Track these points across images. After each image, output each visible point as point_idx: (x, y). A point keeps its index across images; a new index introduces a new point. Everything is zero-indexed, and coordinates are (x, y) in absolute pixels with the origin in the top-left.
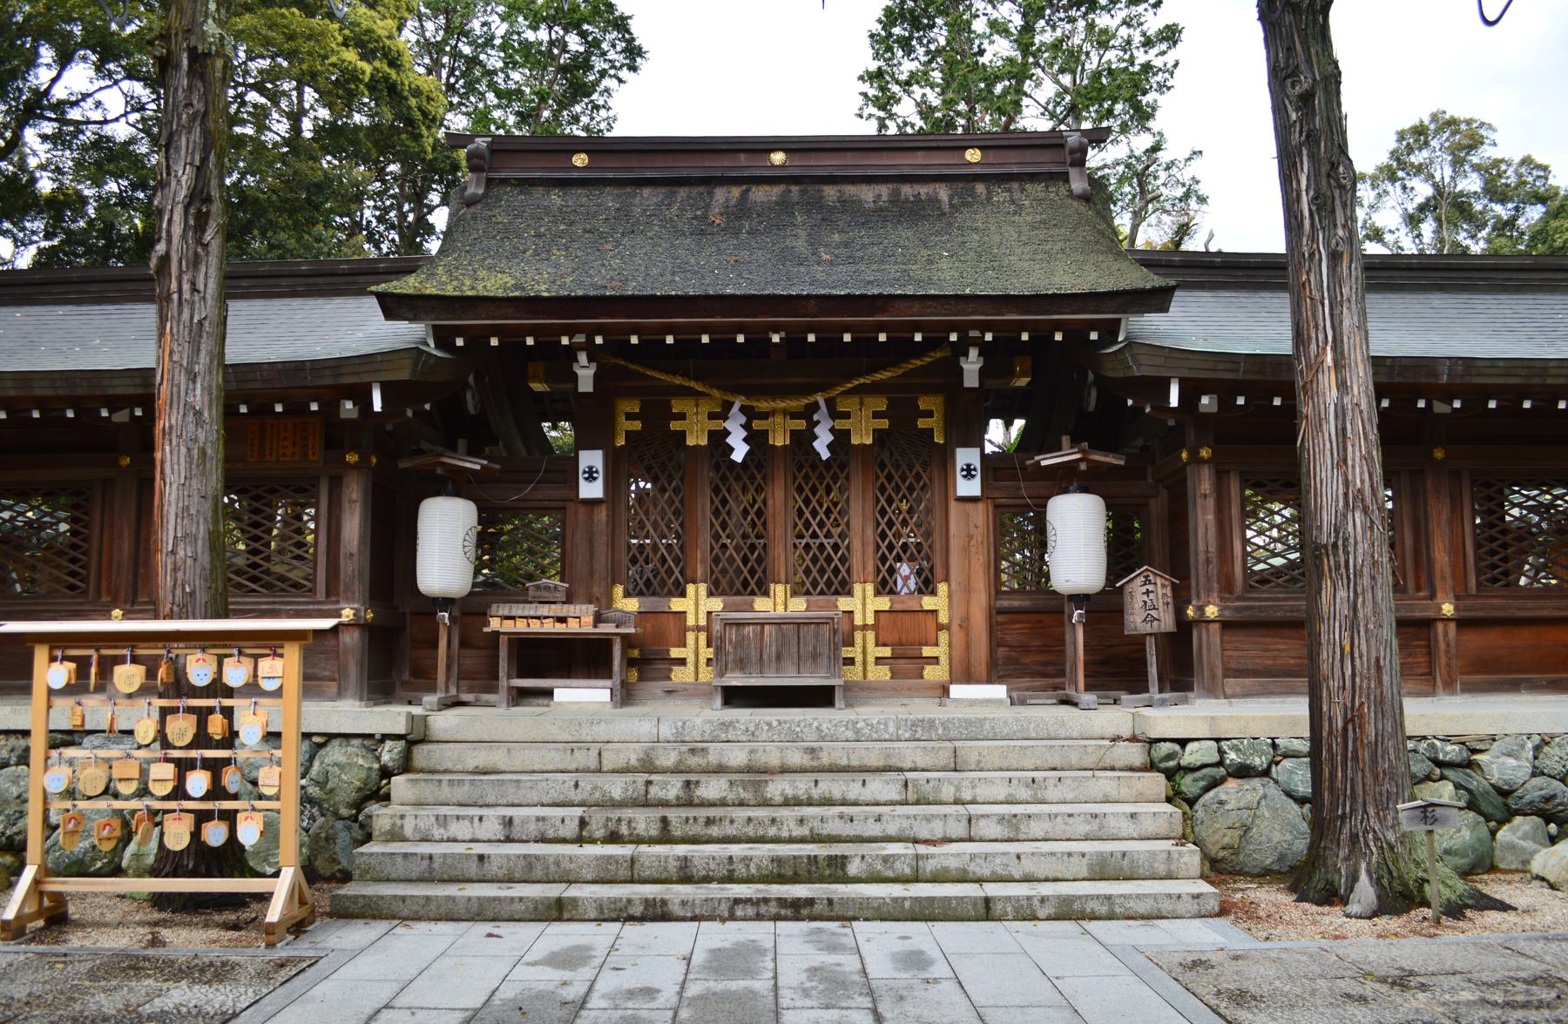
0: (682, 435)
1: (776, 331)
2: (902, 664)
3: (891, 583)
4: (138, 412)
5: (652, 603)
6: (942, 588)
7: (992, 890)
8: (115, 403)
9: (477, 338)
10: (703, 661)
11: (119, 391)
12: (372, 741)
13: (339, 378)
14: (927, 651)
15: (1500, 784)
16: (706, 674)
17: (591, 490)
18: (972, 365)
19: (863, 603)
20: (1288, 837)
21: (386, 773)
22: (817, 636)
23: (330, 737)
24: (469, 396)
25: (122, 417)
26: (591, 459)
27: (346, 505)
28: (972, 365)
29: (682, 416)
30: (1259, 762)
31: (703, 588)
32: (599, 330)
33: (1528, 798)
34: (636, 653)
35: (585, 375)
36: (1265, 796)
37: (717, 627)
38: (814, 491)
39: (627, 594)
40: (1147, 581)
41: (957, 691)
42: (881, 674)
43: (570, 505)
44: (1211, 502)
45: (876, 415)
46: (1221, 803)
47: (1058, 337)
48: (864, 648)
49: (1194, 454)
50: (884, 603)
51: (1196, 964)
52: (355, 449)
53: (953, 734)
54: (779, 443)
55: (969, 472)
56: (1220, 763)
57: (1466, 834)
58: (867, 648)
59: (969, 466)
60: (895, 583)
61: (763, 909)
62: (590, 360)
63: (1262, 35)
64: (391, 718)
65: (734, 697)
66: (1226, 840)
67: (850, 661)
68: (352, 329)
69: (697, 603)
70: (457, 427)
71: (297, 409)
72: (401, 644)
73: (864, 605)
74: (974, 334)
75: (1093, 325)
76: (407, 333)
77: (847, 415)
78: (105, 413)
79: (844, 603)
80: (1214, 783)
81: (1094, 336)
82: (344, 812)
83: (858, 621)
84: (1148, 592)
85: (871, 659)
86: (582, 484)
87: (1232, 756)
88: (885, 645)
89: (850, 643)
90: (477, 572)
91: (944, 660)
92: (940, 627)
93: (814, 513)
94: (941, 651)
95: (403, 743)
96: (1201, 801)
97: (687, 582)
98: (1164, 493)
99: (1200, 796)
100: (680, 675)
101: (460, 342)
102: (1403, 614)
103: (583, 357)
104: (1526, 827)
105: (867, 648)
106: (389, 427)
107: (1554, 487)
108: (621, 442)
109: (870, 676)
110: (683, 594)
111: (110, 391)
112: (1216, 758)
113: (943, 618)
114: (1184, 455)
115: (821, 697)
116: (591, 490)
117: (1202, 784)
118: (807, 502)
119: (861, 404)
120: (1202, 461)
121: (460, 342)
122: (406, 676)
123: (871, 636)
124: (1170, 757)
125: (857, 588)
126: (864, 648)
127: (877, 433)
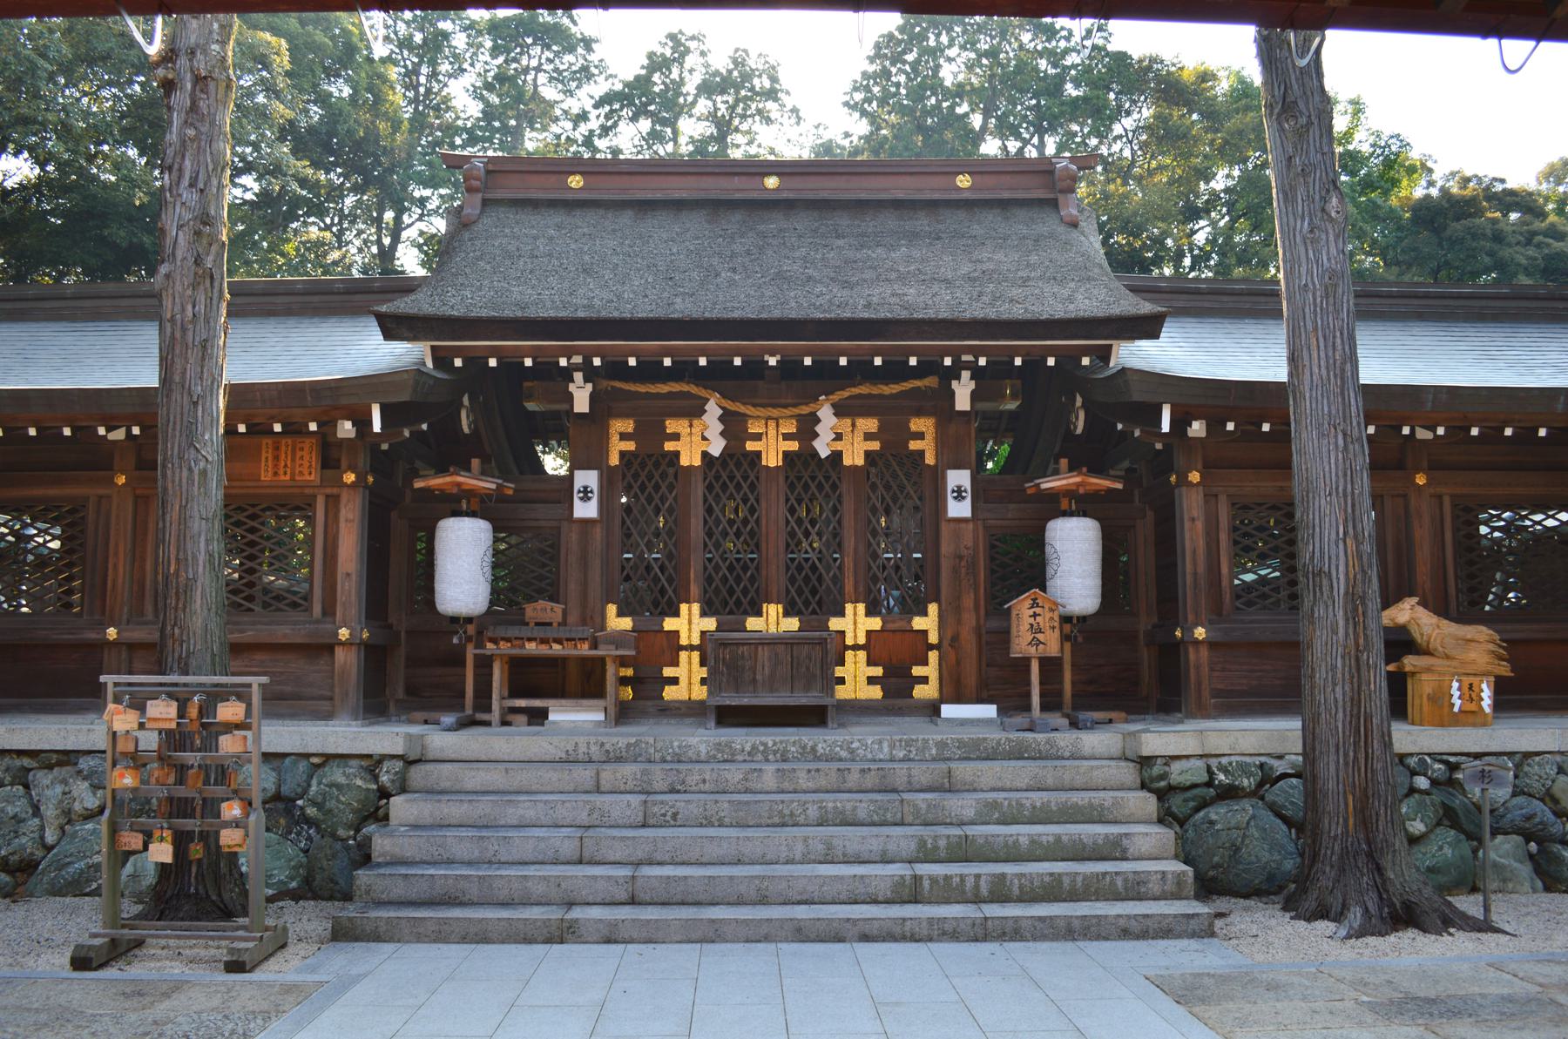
0: (677, 454)
1: (772, 355)
12: (372, 764)
14: (917, 671)
18: (963, 394)
20: (1276, 857)
21: (384, 794)
23: (328, 758)
28: (963, 394)
29: (676, 437)
31: (696, 607)
36: (1253, 817)
45: (868, 437)
49: (1183, 480)
52: (352, 469)
54: (772, 464)
55: (959, 494)
56: (1209, 784)
62: (586, 381)
64: (386, 738)
65: (728, 716)
75: (1086, 351)
80: (1204, 804)
86: (577, 503)
92: (932, 647)
96: (1192, 821)
99: (1191, 816)
103: (578, 376)
104: (1507, 846)
108: (614, 460)
112: (1205, 778)
117: (1192, 804)
119: (853, 425)
120: (1191, 484)
121: (458, 362)
125: (849, 607)
127: (868, 454)
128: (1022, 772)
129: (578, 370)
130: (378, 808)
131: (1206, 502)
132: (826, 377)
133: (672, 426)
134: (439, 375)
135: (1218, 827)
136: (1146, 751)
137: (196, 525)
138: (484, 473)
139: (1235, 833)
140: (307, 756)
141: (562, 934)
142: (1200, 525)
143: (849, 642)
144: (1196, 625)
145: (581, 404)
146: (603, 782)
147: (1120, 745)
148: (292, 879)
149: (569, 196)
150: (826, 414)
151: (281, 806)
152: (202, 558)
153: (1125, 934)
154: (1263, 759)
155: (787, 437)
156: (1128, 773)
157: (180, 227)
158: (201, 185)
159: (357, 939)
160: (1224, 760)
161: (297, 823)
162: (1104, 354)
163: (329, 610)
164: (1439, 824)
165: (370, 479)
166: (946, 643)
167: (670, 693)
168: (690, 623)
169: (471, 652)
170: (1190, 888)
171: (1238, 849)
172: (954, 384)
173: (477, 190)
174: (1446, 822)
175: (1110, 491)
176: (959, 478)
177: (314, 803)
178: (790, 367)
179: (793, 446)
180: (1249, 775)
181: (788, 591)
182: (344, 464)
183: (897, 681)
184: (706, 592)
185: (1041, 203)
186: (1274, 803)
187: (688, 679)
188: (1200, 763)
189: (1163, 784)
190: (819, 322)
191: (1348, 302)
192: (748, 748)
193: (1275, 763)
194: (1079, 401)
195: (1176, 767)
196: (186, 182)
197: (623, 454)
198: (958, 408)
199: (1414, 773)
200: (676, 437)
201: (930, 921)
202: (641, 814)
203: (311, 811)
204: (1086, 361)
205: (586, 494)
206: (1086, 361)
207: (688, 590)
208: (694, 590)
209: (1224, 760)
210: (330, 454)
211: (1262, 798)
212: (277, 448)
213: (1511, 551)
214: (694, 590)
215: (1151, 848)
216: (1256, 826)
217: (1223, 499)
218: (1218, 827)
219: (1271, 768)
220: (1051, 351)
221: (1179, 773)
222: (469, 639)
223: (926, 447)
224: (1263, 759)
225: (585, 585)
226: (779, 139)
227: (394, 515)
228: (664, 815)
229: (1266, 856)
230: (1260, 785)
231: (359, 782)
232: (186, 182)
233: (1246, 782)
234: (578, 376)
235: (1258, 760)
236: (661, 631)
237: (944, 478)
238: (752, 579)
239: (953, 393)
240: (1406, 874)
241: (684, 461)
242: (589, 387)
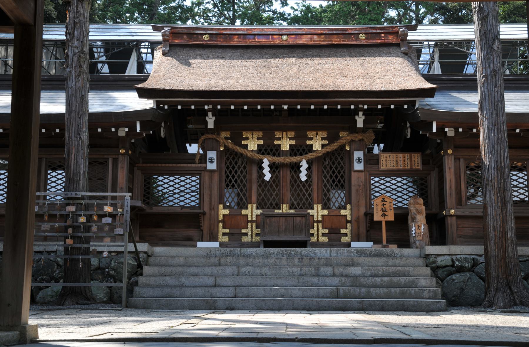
1: (286, 105)
3: (328, 204)
9: (172, 106)
13: (127, 118)
14: (343, 231)
19: (318, 212)
20: (479, 293)
24: (162, 130)
31: (254, 206)
35: (211, 123)
36: (470, 278)
41: (354, 244)
47: (392, 107)
48: (318, 210)
50: (325, 212)
56: (453, 266)
59: (359, 158)
60: (330, 204)
62: (213, 116)
63: (146, 99)
65: (268, 244)
68: (129, 101)
73: (318, 212)
76: (148, 104)
80: (451, 274)
86: (208, 164)
88: (326, 229)
91: (349, 234)
92: (348, 222)
94: (347, 231)
96: (446, 280)
97: (248, 203)
98: (436, 169)
99: (446, 278)
112: (451, 263)
113: (349, 218)
116: (212, 166)
117: (446, 273)
119: (317, 134)
120: (448, 154)
125: (315, 206)
126: (318, 210)
128: (381, 261)
129: (210, 111)
130: (137, 272)
131: (455, 162)
135: (456, 281)
136: (427, 253)
139: (462, 284)
142: (453, 170)
144: (451, 209)
145: (211, 124)
146: (222, 262)
147: (419, 253)
148: (105, 297)
149: (205, 43)
151: (99, 271)
154: (474, 256)
156: (420, 261)
158: (81, 40)
160: (458, 257)
161: (106, 277)
165: (130, 152)
166: (353, 220)
167: (245, 239)
168: (252, 212)
170: (440, 296)
171: (463, 290)
172: (356, 117)
176: (358, 154)
177: (113, 269)
178: (292, 111)
181: (291, 200)
182: (120, 146)
183: (334, 234)
184: (258, 200)
186: (478, 272)
187: (250, 233)
188: (448, 257)
189: (434, 265)
191: (500, 82)
192: (276, 253)
193: (479, 258)
194: (408, 125)
195: (439, 259)
196: (76, 39)
198: (358, 126)
202: (237, 272)
203: (112, 272)
205: (211, 161)
206: (406, 107)
208: (254, 198)
209: (458, 257)
211: (473, 271)
214: (254, 198)
215: (426, 281)
216: (471, 281)
217: (462, 160)
218: (456, 281)
219: (477, 260)
221: (440, 261)
224: (474, 256)
225: (211, 196)
228: (245, 272)
229: (475, 292)
230: (473, 266)
231: (130, 262)
232: (76, 39)
233: (467, 265)
234: (210, 114)
235: (472, 257)
236: (241, 215)
238: (277, 195)
239: (356, 120)
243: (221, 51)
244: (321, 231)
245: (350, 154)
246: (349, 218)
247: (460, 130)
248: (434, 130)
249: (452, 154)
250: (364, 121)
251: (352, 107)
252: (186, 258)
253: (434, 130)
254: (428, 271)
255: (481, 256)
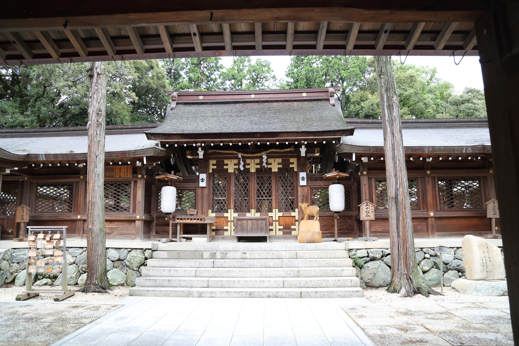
0: (227, 169)
2: (286, 230)
4: (85, 164)
5: (219, 214)
6: (297, 210)
7: (303, 290)
8: (79, 162)
9: (172, 145)
10: (232, 230)
11: (80, 159)
12: (144, 250)
15: (445, 261)
16: (233, 233)
17: (203, 184)
18: (303, 150)
20: (386, 276)
21: (146, 259)
22: (253, 224)
23: (132, 249)
24: (171, 159)
25: (81, 165)
26: (203, 176)
27: (138, 188)
28: (303, 150)
29: (227, 165)
30: (378, 256)
31: (232, 210)
32: (203, 142)
33: (453, 265)
34: (214, 228)
35: (201, 154)
36: (380, 265)
37: (235, 220)
38: (262, 184)
39: (213, 212)
40: (367, 205)
42: (281, 233)
43: (197, 188)
44: (367, 186)
45: (279, 164)
46: (368, 267)
49: (362, 173)
51: (352, 309)
52: (140, 174)
53: (296, 249)
54: (253, 171)
55: (303, 179)
56: (368, 256)
57: (435, 275)
58: (276, 227)
61: (241, 294)
62: (202, 150)
64: (147, 244)
65: (241, 239)
66: (369, 277)
67: (272, 230)
69: (231, 214)
70: (168, 168)
71: (125, 164)
72: (157, 224)
74: (303, 142)
75: (334, 139)
76: (152, 143)
77: (271, 164)
78: (76, 164)
79: (270, 214)
81: (334, 142)
82: (135, 269)
83: (274, 219)
84: (367, 208)
85: (277, 229)
87: (371, 255)
89: (272, 225)
90: (177, 206)
92: (296, 221)
93: (262, 190)
95: (150, 251)
100: (226, 234)
101: (167, 146)
102: (413, 216)
103: (200, 149)
104: (452, 273)
105: (276, 227)
106: (150, 168)
107: (468, 181)
108: (211, 171)
109: (277, 234)
110: (227, 212)
111: (77, 159)
112: (367, 255)
113: (297, 218)
114: (359, 174)
115: (263, 239)
116: (203, 184)
118: (260, 187)
120: (364, 175)
121: (167, 146)
122: (154, 234)
123: (277, 223)
124: (354, 255)
125: (274, 210)
127: (279, 169)
132: (264, 147)
133: (226, 162)
134: (162, 149)
137: (96, 188)
138: (175, 174)
140: (127, 249)
141: (189, 295)
143: (274, 219)
150: (265, 157)
152: (98, 196)
153: (339, 296)
155: (257, 164)
156: (346, 254)
157: (93, 112)
159: (135, 295)
160: (372, 250)
162: (339, 139)
163: (134, 211)
164: (432, 267)
169: (171, 222)
173: (175, 100)
174: (434, 266)
175: (346, 177)
176: (303, 174)
179: (259, 166)
180: (379, 254)
182: (138, 172)
185: (325, 100)
188: (365, 251)
190: (261, 133)
195: (358, 251)
197: (213, 169)
199: (425, 253)
200: (227, 165)
201: (286, 292)
203: (127, 263)
204: (334, 142)
205: (203, 180)
207: (230, 206)
210: (135, 171)
212: (120, 169)
213: (467, 193)
214: (232, 206)
220: (324, 139)
222: (171, 219)
223: (295, 166)
224: (383, 250)
226: (270, 85)
227: (153, 186)
229: (383, 276)
230: (382, 257)
237: (299, 174)
240: (421, 280)
241: (229, 171)
242: (203, 151)
243: (196, 105)
244: (278, 227)
245: (297, 174)
246: (297, 218)
247: (372, 159)
248: (354, 159)
249: (366, 175)
250: (306, 152)
251: (296, 143)
252: (141, 275)
253: (354, 159)
254: (350, 262)
255: (387, 249)
